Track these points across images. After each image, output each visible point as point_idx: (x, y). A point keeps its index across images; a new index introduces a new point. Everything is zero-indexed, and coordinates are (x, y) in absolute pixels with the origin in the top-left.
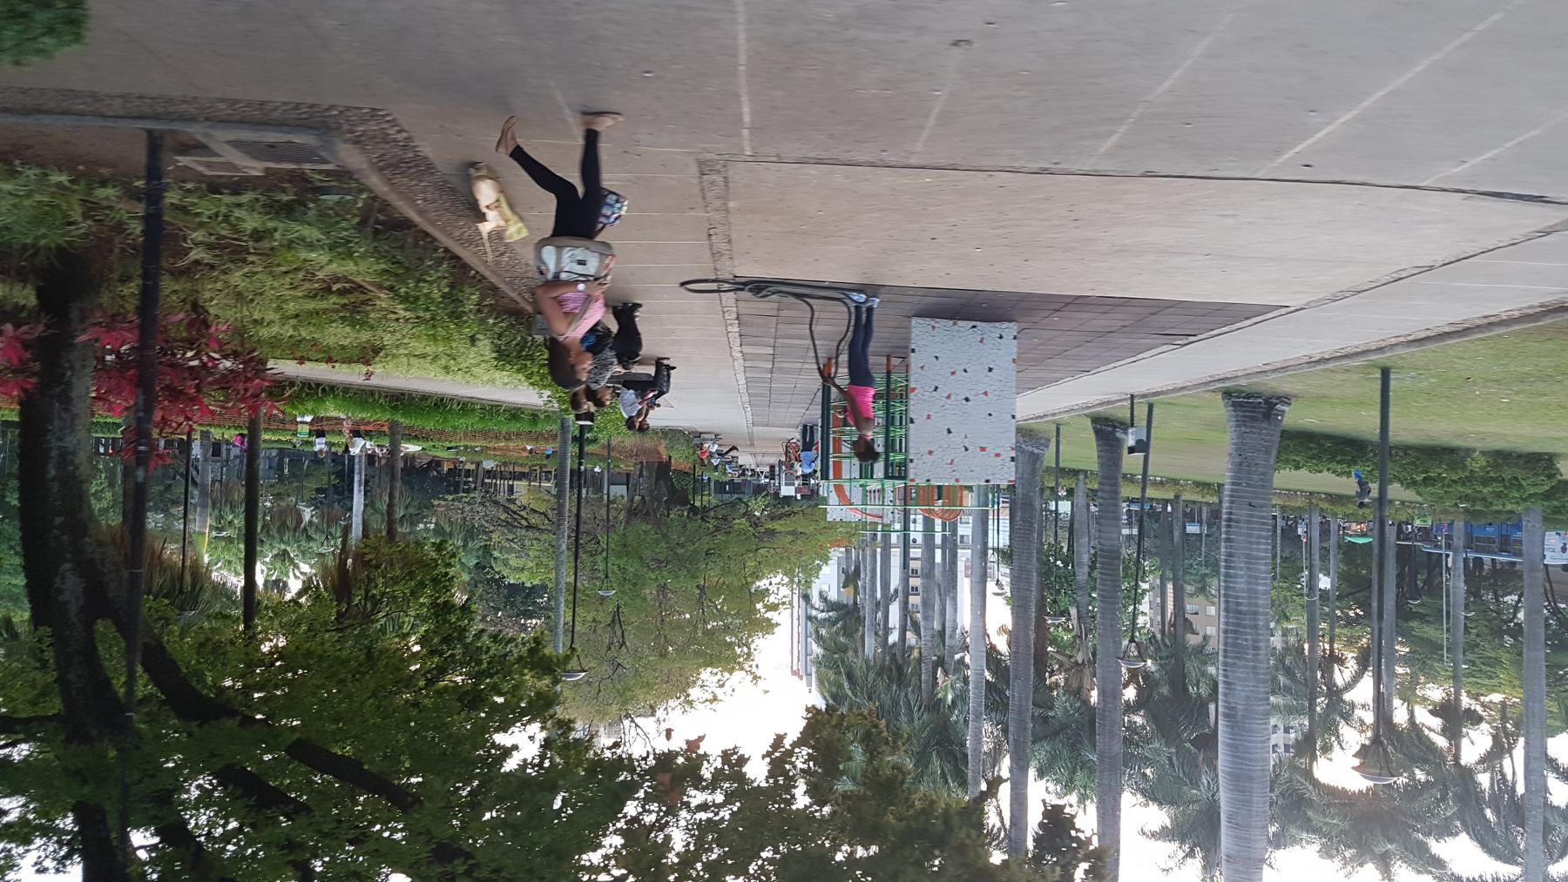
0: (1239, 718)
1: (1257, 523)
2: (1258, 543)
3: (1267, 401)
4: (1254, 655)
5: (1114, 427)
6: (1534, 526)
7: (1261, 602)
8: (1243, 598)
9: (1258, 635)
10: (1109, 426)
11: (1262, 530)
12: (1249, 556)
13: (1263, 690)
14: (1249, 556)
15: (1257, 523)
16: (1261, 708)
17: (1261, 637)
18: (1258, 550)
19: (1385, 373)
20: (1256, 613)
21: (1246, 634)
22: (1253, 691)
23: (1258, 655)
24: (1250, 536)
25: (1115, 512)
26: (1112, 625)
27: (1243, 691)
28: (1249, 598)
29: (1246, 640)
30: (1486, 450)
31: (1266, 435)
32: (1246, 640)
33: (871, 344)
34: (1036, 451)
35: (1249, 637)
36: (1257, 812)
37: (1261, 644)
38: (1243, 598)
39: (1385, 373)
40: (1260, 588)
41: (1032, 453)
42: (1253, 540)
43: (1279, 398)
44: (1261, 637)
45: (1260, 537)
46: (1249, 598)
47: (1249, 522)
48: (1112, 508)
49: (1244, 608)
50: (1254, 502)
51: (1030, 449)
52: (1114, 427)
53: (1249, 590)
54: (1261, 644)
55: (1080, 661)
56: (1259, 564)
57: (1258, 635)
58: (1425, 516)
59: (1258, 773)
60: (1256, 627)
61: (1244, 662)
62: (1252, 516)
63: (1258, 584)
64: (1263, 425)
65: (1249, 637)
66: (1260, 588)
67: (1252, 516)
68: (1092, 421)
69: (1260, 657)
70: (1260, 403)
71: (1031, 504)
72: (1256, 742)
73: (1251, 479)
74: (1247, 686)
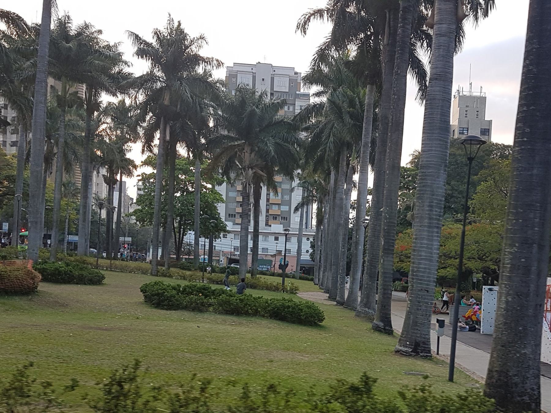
0: (443, 166)
1: (425, 281)
2: (425, 268)
3: (418, 353)
4: (432, 202)
5: (384, 329)
6: (34, 250)
7: (426, 233)
8: (435, 236)
9: (429, 214)
10: (387, 330)
11: (422, 276)
12: (431, 261)
13: (428, 181)
14: (431, 261)
15: (425, 281)
16: (431, 171)
17: (427, 212)
18: (425, 264)
19: (451, 379)
20: (429, 227)
21: (436, 215)
22: (435, 181)
23: (430, 202)
24: (429, 273)
25: (385, 277)
26: (392, 210)
27: (440, 181)
28: (432, 236)
29: (436, 211)
30: (17, 301)
31: (417, 333)
32: (436, 211)
33: (448, 370)
34: (367, 309)
35: (434, 213)
36: (438, 109)
37: (427, 208)
38: (435, 236)
39: (451, 379)
40: (426, 242)
41: (369, 308)
42: (428, 271)
43: (411, 355)
44: (427, 212)
45: (424, 272)
46: (432, 236)
47: (429, 281)
48: (387, 280)
49: (435, 230)
50: (426, 293)
51: (370, 311)
52: (384, 329)
53: (432, 240)
54: (427, 208)
55: (250, 169)
56: (426, 256)
57: (429, 214)
58: (23, 251)
59: (437, 132)
60: (430, 219)
61: (438, 198)
62: (427, 285)
63: (427, 244)
64: (420, 339)
65: (434, 213)
66: (426, 242)
67: (427, 285)
68: (392, 331)
69: (428, 201)
70: (421, 353)
71: (370, 277)
72: (435, 150)
73: (426, 307)
74: (438, 184)
